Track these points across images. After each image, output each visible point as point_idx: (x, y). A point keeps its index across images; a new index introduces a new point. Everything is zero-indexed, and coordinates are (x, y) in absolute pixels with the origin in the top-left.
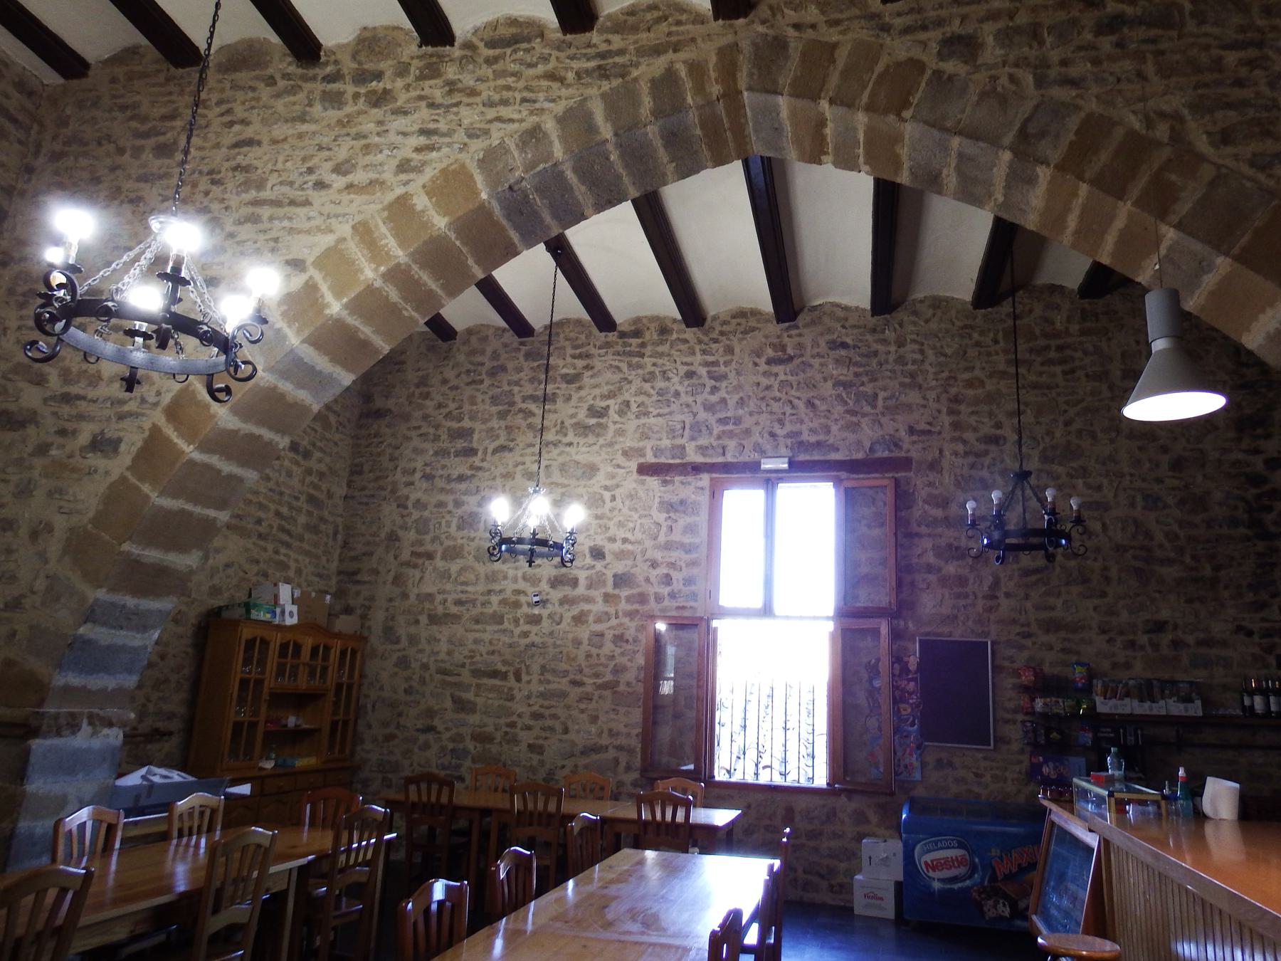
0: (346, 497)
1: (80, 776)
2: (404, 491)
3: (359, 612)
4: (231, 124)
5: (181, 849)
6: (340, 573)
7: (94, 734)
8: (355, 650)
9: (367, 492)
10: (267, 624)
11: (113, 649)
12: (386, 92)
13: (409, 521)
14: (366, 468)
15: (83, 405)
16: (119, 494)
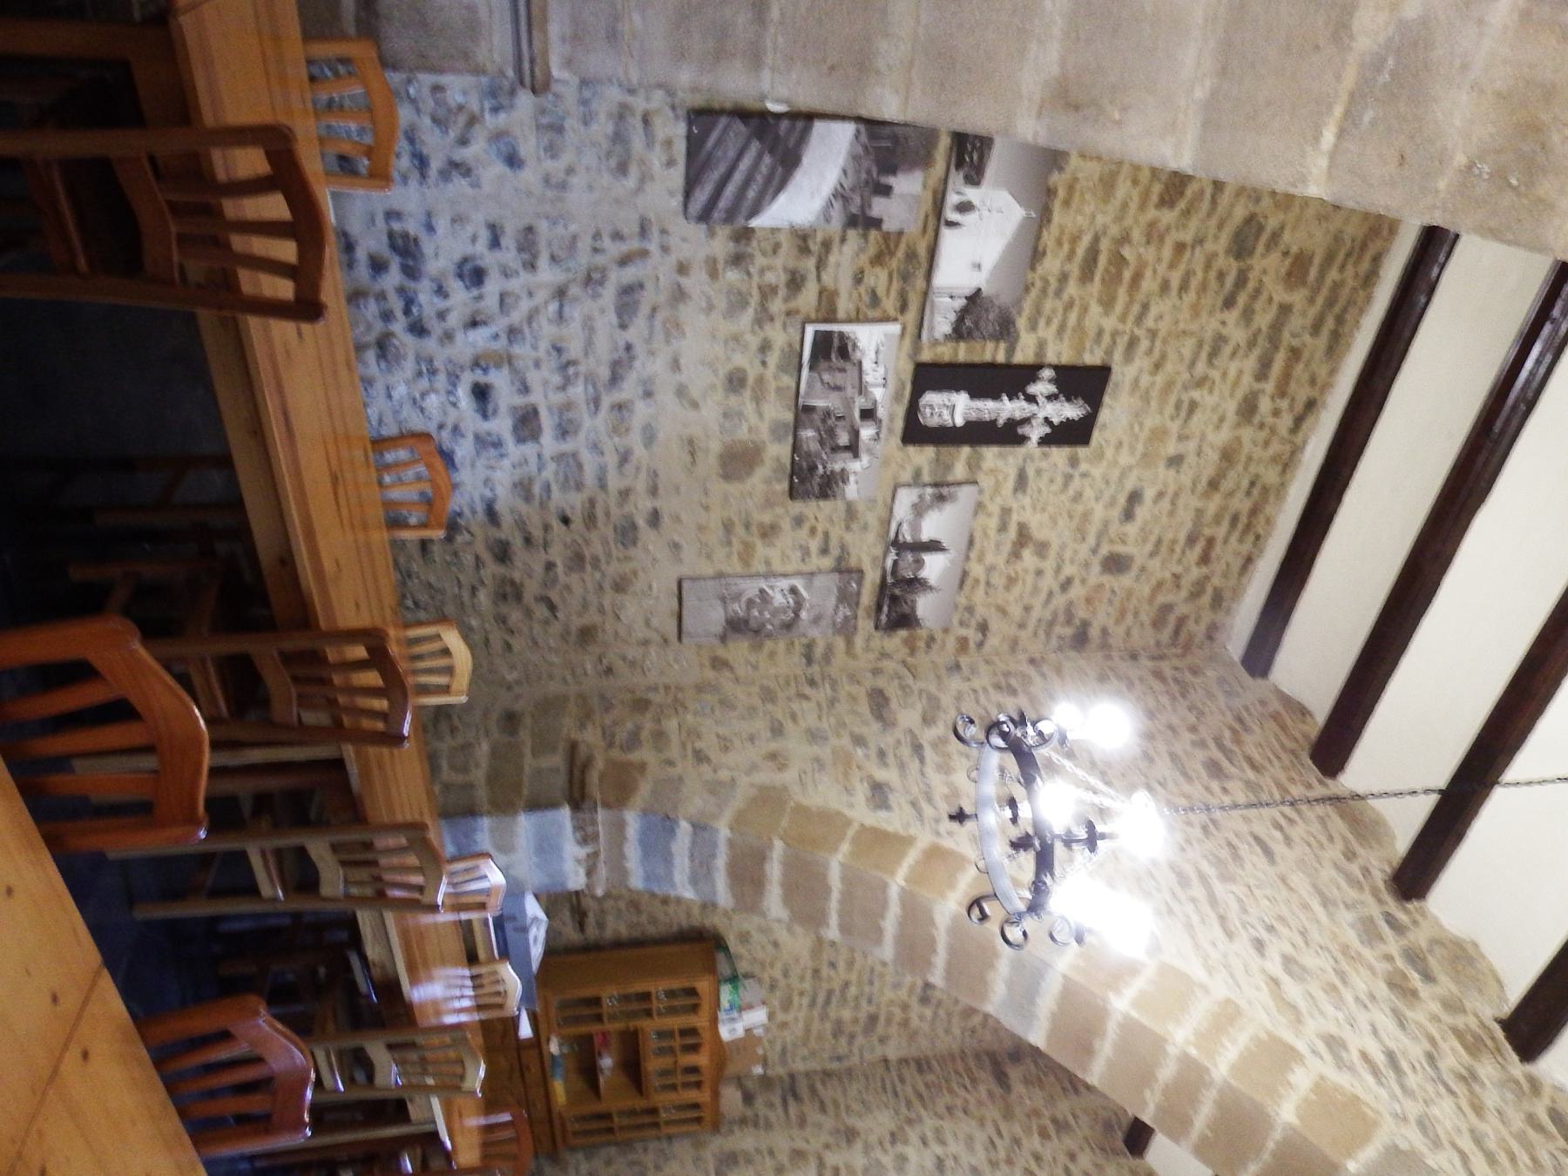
0: (886, 1061)
1: (535, 859)
2: (913, 1135)
3: (749, 1113)
4: (1279, 827)
5: (459, 982)
6: (792, 1077)
7: (578, 861)
8: (702, 1119)
9: (899, 1088)
10: (717, 1004)
11: (668, 858)
12: (1415, 993)
13: (878, 1153)
14: (930, 1078)
15: (914, 765)
16: (832, 823)
